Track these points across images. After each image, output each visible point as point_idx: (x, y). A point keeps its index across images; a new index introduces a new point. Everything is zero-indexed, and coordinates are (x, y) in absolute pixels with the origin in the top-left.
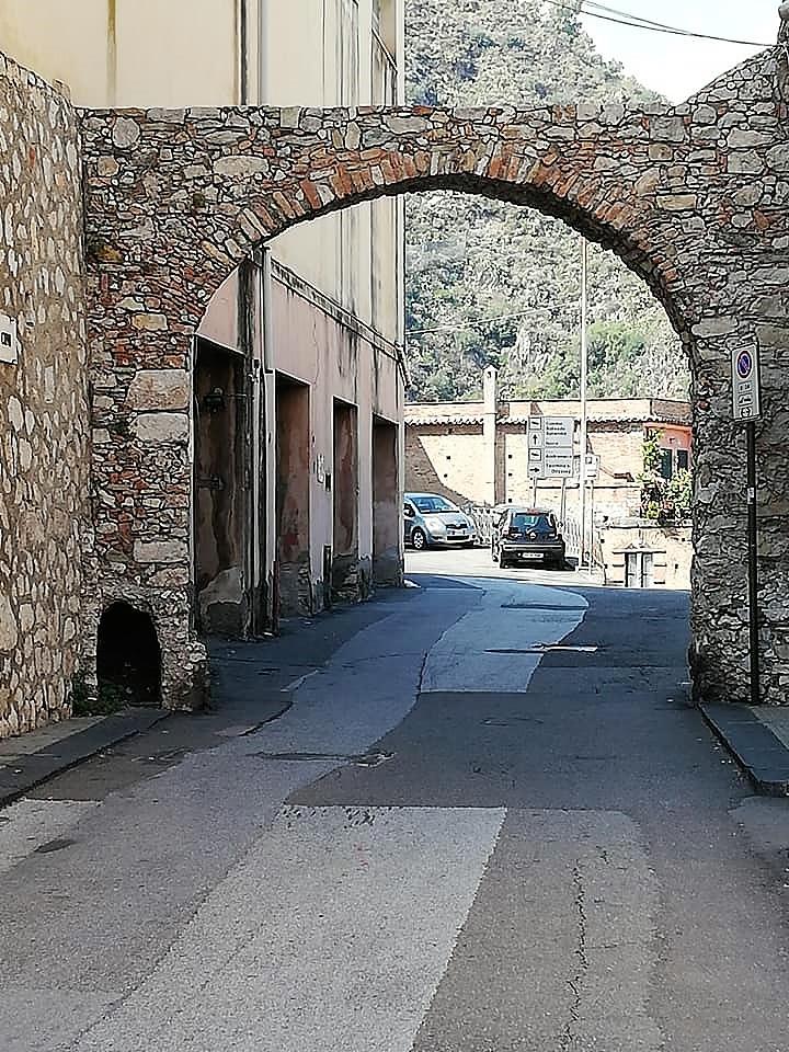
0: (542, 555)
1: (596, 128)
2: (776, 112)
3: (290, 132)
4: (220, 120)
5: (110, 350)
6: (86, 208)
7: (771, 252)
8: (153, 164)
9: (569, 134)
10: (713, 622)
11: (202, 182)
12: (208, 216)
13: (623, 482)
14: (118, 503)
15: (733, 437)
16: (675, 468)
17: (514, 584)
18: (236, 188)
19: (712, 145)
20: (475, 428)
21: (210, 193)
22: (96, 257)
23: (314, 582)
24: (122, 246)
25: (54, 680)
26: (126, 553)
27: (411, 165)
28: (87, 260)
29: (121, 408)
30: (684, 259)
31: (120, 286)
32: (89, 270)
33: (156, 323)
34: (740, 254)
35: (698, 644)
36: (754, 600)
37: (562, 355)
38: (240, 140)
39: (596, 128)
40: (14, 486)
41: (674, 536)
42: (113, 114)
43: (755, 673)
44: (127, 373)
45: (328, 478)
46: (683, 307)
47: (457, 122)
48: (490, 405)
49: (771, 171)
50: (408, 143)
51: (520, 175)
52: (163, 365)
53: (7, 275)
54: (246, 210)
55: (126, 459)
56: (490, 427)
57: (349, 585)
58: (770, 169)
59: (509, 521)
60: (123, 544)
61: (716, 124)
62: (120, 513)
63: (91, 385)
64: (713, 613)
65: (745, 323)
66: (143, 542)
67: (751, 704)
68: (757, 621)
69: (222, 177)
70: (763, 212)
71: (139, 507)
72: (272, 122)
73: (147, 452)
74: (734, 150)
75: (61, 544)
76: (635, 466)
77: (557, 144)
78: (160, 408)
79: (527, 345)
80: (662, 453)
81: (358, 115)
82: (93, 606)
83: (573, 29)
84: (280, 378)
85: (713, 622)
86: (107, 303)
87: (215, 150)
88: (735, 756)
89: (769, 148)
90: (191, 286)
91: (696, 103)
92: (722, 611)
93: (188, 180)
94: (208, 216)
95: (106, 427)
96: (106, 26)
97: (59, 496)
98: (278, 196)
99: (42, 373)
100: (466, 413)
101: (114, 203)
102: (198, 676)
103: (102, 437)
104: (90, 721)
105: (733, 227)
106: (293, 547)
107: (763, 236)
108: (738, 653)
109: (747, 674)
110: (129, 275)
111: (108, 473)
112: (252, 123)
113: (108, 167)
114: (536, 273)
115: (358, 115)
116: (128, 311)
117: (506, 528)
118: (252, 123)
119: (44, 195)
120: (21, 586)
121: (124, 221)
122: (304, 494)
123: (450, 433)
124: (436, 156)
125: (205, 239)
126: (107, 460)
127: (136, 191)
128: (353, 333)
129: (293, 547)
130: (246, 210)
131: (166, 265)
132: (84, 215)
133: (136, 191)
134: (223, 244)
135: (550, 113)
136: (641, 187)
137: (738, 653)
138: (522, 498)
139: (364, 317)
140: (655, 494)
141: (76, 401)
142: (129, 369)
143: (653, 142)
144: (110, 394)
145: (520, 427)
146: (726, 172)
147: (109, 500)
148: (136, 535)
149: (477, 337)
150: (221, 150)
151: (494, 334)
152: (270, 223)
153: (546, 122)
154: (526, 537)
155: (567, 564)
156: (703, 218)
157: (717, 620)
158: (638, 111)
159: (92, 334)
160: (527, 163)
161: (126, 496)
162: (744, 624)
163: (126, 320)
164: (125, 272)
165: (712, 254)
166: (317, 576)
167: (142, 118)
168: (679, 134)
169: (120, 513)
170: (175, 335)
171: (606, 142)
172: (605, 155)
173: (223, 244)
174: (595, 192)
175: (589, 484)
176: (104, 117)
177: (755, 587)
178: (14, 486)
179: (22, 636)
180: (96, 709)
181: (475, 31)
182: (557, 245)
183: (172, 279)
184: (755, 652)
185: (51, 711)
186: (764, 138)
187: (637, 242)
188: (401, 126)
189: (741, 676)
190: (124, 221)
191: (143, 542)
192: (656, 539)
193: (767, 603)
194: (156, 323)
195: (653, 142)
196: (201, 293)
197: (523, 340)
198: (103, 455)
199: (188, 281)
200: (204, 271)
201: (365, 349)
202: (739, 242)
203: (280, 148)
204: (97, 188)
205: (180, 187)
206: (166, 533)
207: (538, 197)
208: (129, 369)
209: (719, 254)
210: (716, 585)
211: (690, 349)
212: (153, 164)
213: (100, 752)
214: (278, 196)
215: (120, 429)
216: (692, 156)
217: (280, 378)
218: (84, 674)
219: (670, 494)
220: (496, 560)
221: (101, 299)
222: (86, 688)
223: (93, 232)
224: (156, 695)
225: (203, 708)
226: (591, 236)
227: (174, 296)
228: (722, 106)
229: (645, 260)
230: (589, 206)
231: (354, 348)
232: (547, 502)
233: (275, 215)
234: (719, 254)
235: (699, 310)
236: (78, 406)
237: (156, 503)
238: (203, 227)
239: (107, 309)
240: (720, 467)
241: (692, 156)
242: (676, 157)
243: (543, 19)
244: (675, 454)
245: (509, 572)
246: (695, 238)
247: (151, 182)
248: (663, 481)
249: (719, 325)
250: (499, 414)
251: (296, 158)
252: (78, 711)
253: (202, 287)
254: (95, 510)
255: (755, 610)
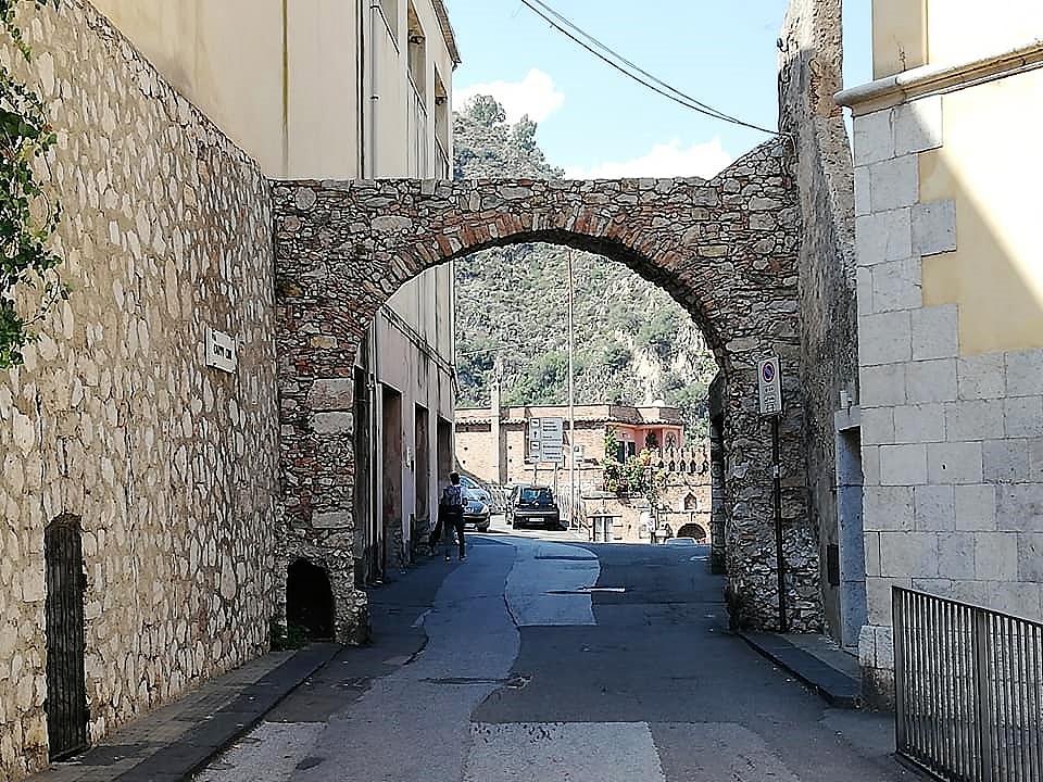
0: (543, 520)
1: (653, 196)
2: (783, 184)
3: (428, 198)
4: (376, 189)
5: (294, 364)
6: (276, 256)
7: (782, 288)
8: (326, 222)
9: (634, 200)
10: (748, 569)
11: (363, 236)
12: (368, 261)
13: (591, 465)
14: (300, 482)
15: (758, 428)
16: (626, 455)
17: (530, 541)
18: (388, 240)
19: (738, 208)
20: (485, 427)
21: (369, 244)
22: (284, 292)
23: (405, 542)
24: (304, 284)
25: (259, 623)
26: (306, 521)
27: (518, 222)
28: (277, 296)
29: (302, 408)
30: (720, 293)
31: (302, 315)
32: (278, 302)
33: (329, 343)
34: (761, 290)
35: (736, 587)
36: (780, 551)
37: (526, 375)
38: (391, 204)
39: (653, 196)
40: (233, 469)
41: (627, 504)
42: (296, 184)
43: (782, 608)
44: (308, 382)
45: (412, 462)
46: (720, 330)
47: (551, 191)
48: (495, 411)
49: (781, 228)
50: (515, 206)
51: (598, 230)
52: (335, 375)
53: (228, 305)
54: (396, 257)
55: (307, 448)
56: (495, 427)
57: (423, 543)
58: (781, 226)
59: (519, 495)
60: (303, 513)
61: (740, 193)
62: (301, 490)
63: (279, 392)
64: (748, 563)
65: (765, 341)
66: (320, 512)
67: (780, 632)
68: (782, 568)
69: (378, 231)
70: (776, 258)
71: (316, 484)
72: (416, 191)
73: (322, 442)
74: (754, 212)
75: (262, 514)
76: (600, 455)
77: (625, 209)
78: (332, 408)
79: (501, 369)
80: (618, 444)
81: (479, 186)
82: (284, 563)
83: (530, 146)
84: (386, 389)
85: (748, 569)
86: (292, 328)
87: (370, 212)
88: (796, 675)
89: (779, 211)
90: (355, 315)
91: (726, 178)
92: (755, 560)
93: (352, 234)
94: (368, 261)
95: (291, 423)
96: (282, 122)
97: (260, 477)
98: (420, 246)
99: (250, 380)
100: (478, 416)
101: (297, 252)
102: (362, 616)
103: (288, 431)
104: (285, 656)
105: (754, 270)
106: (390, 516)
107: (776, 276)
108: (768, 593)
109: (776, 610)
110: (309, 306)
111: (293, 459)
112: (399, 191)
113: (293, 222)
114: (507, 317)
115: (479, 186)
116: (308, 334)
117: (518, 499)
118: (399, 191)
119: (250, 244)
120: (238, 549)
121: (304, 265)
122: (398, 479)
123: (467, 431)
124: (536, 216)
125: (366, 279)
126: (292, 449)
127: (313, 243)
128: (425, 355)
129: (390, 516)
130: (396, 257)
131: (336, 298)
132: (275, 261)
133: (313, 243)
134: (378, 282)
135: (620, 184)
136: (686, 240)
137: (768, 593)
138: (520, 477)
139: (432, 344)
140: (614, 473)
141: (269, 407)
142: (308, 379)
143: (694, 206)
144: (293, 398)
145: (516, 426)
146: (748, 229)
147: (294, 480)
148: (313, 507)
149: (467, 362)
150: (376, 212)
151: (479, 361)
152: (414, 267)
153: (617, 191)
154: (532, 507)
155: (561, 526)
156: (733, 262)
157: (751, 567)
158: (684, 183)
159: (280, 352)
160: (604, 221)
161: (307, 476)
162: (772, 570)
163: (306, 341)
164: (304, 304)
165: (739, 289)
166: (407, 538)
167: (318, 187)
168: (713, 201)
169: (301, 490)
170: (343, 352)
171: (660, 206)
172: (660, 216)
173: (378, 282)
174: (654, 243)
175: (577, 467)
176: (289, 187)
177: (780, 542)
178: (233, 469)
179: (238, 587)
180: (289, 645)
181: (463, 147)
182: (521, 297)
183: (341, 310)
184: (782, 591)
185: (257, 647)
186: (775, 204)
187: (685, 281)
188: (512, 194)
189: (771, 611)
190: (304, 265)
191: (320, 512)
192: (614, 507)
193: (789, 554)
194: (329, 343)
195: (694, 206)
196: (363, 320)
197: (498, 364)
198: (288, 445)
199: (352, 311)
200: (364, 303)
201: (433, 367)
202: (759, 280)
203: (420, 210)
204: (284, 240)
205: (346, 239)
206: (337, 505)
207: (611, 248)
208: (308, 379)
209: (746, 290)
210: (749, 540)
211: (723, 362)
212: (326, 222)
213: (305, 680)
214: (420, 246)
215: (302, 425)
216: (723, 217)
217: (386, 389)
218: (278, 616)
219: (625, 474)
220: (509, 523)
221: (287, 325)
222: (280, 628)
223: (281, 274)
224: (329, 632)
225: (366, 642)
226: (647, 276)
227: (343, 322)
228: (745, 179)
229: (690, 294)
230: (649, 254)
231: (426, 367)
232: (545, 480)
233: (417, 261)
234: (746, 290)
235: (731, 332)
236: (272, 407)
237: (330, 482)
238: (364, 270)
239: (292, 332)
240: (749, 450)
241: (723, 217)
242: (712, 218)
243: (509, 139)
244: (626, 444)
245: (519, 532)
246: (727, 278)
247: (325, 236)
248: (619, 464)
249: (746, 344)
250: (502, 418)
251: (433, 218)
252: (275, 647)
253: (363, 315)
254: (283, 488)
255: (781, 559)
